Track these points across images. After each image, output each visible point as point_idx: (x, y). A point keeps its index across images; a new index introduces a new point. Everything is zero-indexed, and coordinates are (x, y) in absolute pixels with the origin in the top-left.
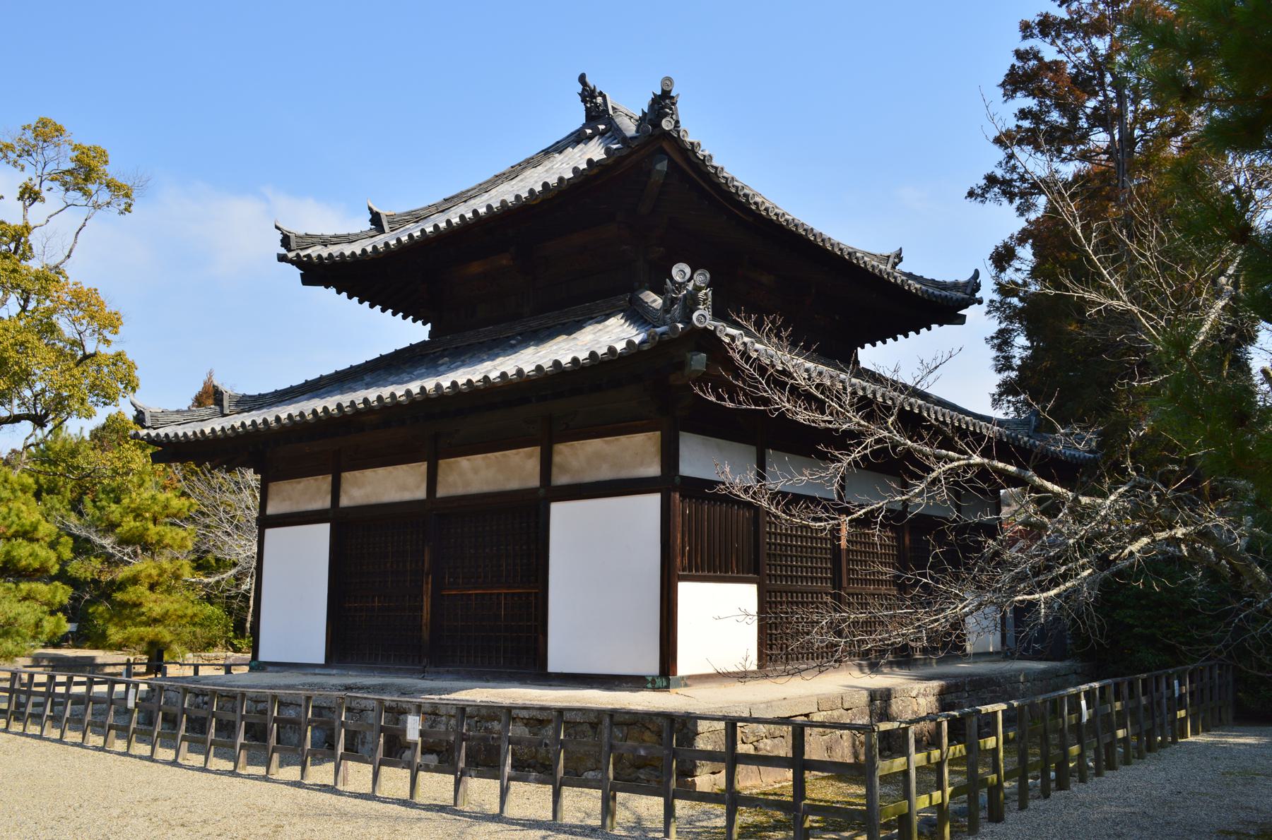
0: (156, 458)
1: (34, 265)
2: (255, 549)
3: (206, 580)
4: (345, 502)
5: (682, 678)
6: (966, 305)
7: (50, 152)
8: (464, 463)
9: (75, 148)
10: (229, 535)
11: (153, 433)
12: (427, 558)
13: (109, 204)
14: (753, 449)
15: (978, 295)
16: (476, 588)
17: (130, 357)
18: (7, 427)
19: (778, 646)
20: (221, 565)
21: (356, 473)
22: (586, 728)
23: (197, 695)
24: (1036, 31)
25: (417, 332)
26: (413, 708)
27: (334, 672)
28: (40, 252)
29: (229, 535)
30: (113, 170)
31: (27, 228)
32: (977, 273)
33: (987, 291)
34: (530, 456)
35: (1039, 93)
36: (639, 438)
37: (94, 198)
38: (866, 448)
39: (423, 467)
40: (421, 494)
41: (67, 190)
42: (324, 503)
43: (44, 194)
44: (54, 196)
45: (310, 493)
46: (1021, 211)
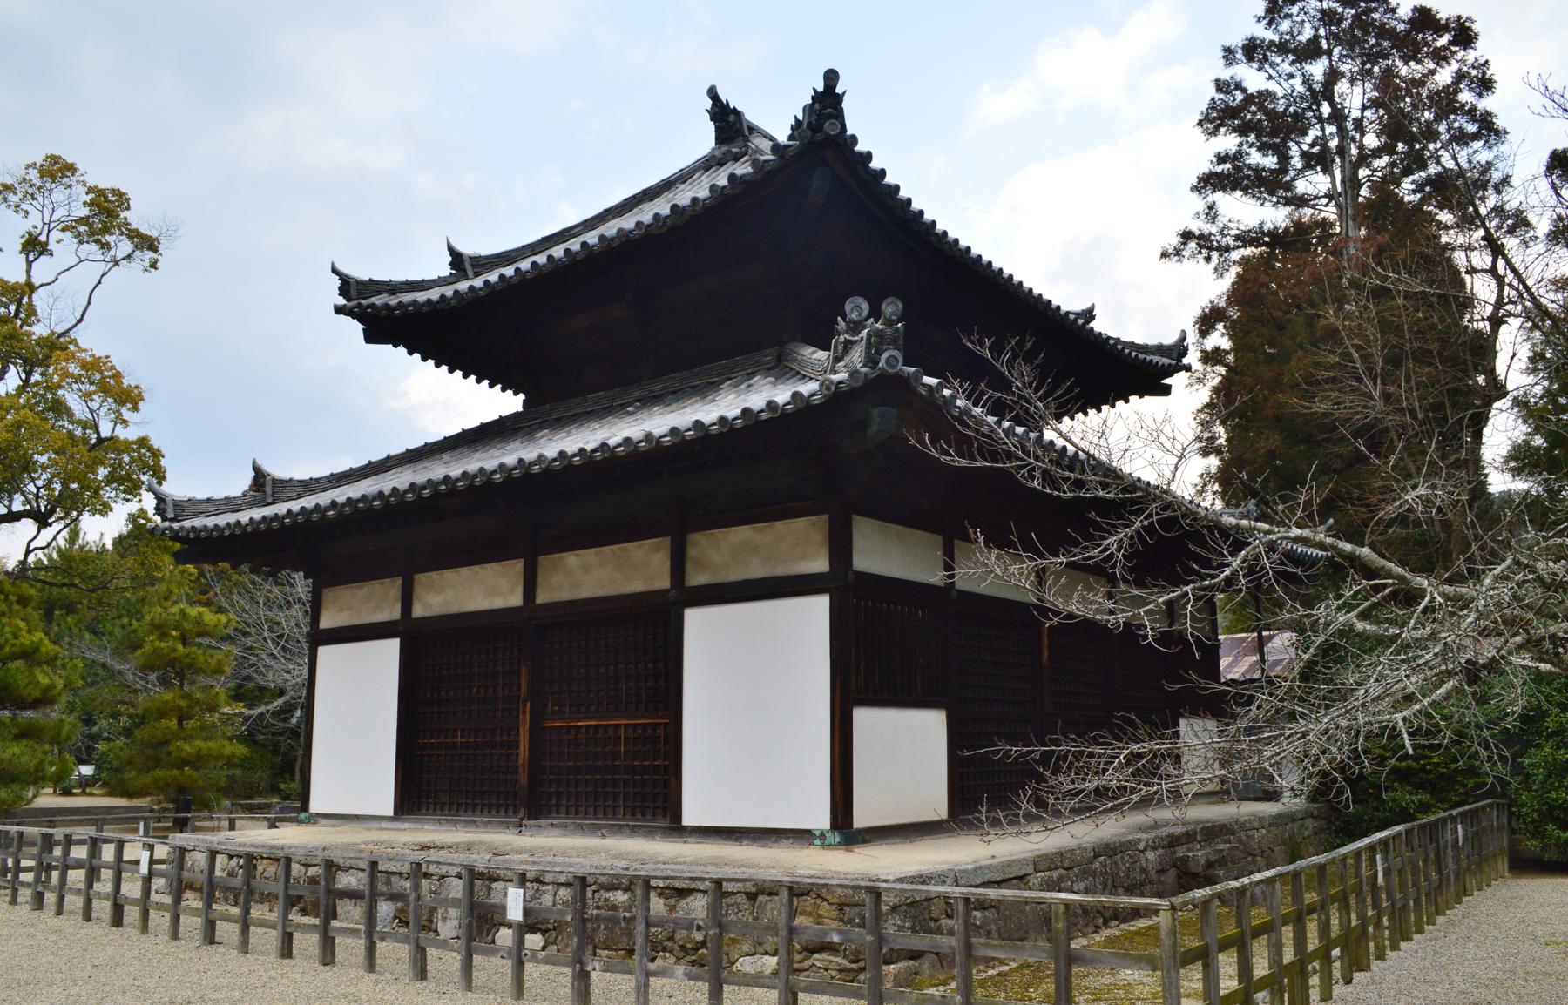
0: (180, 558)
1: (39, 331)
2: (305, 672)
3: (247, 712)
4: (418, 611)
5: (860, 831)
6: (1171, 371)
7: (59, 194)
8: (572, 559)
9: (90, 190)
10: (275, 658)
11: (176, 526)
12: (524, 682)
13: (129, 257)
14: (939, 539)
15: (1185, 361)
16: (585, 718)
17: (155, 443)
18: (4, 525)
19: (978, 792)
20: (261, 694)
21: (434, 575)
22: (741, 898)
23: (231, 857)
24: (1239, 55)
25: (510, 403)
26: (515, 878)
27: (406, 825)
28: (46, 315)
29: (275, 658)
30: (136, 217)
31: (31, 288)
32: (1184, 337)
33: (1192, 358)
34: (657, 549)
35: (1242, 131)
36: (800, 523)
37: (112, 252)
38: (1150, 515)
39: (519, 565)
40: (516, 600)
41: (81, 242)
42: (392, 613)
43: (52, 246)
44: (64, 248)
45: (376, 601)
46: (1220, 272)
